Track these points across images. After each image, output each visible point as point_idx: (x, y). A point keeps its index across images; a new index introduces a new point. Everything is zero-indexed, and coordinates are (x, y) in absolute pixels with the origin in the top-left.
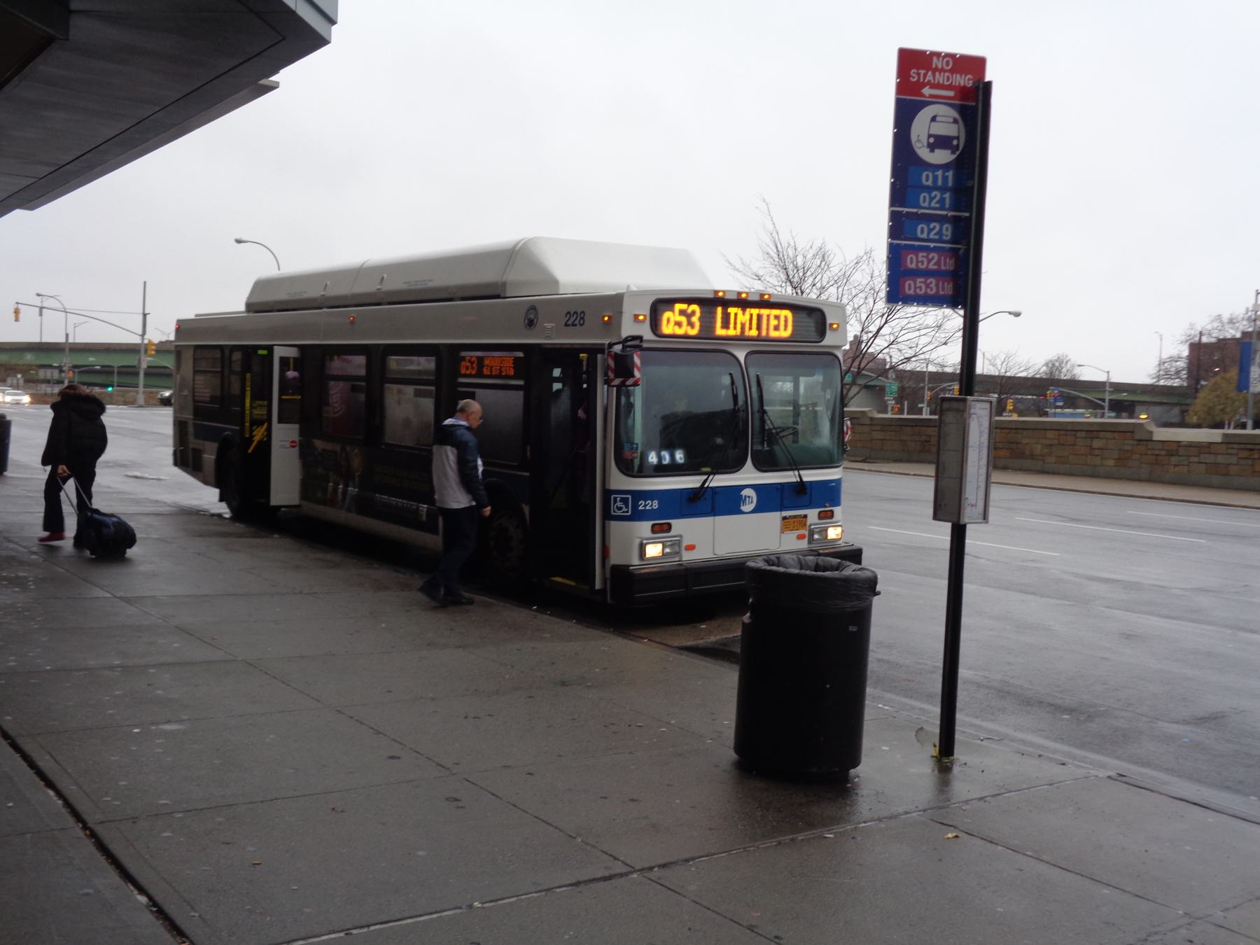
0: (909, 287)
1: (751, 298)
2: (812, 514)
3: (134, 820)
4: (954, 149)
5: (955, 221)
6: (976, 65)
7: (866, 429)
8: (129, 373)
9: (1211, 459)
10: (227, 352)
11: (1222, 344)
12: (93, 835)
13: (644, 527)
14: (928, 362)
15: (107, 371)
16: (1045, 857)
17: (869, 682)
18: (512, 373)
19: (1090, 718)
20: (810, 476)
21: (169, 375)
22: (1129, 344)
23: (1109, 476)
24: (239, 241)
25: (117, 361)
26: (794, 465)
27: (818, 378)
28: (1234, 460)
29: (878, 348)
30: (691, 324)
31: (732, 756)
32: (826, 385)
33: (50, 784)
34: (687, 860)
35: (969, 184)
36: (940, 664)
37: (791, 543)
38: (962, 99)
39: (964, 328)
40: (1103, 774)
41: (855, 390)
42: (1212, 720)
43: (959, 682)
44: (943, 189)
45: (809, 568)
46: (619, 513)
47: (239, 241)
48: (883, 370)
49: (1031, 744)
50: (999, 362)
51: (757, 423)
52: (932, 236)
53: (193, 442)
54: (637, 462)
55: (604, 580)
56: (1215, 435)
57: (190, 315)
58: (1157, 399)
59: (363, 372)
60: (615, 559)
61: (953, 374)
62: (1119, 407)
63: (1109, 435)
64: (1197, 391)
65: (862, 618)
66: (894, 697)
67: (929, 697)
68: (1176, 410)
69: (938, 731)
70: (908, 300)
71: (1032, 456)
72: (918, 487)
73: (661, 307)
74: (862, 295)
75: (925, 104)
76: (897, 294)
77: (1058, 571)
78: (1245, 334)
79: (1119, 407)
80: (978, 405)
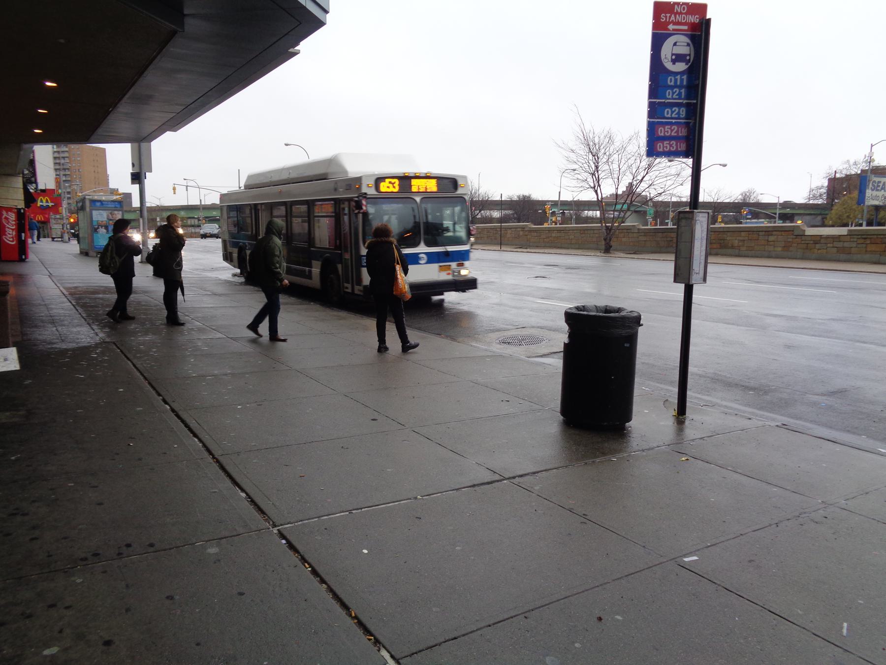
0: (660, 147)
3: (238, 453)
4: (687, 62)
5: (688, 106)
6: (703, 8)
7: (635, 235)
9: (840, 245)
11: (848, 178)
12: (218, 461)
14: (672, 195)
16: (739, 471)
19: (766, 393)
22: (792, 181)
24: (287, 145)
28: (854, 245)
29: (643, 189)
33: (195, 435)
34: (534, 473)
38: (692, 31)
40: (773, 424)
41: (628, 213)
42: (840, 393)
44: (680, 87)
47: (287, 145)
48: (646, 201)
49: (731, 408)
53: (230, 249)
56: (843, 231)
61: (686, 202)
62: (784, 217)
63: (779, 233)
64: (832, 205)
65: (632, 339)
66: (652, 383)
68: (819, 218)
70: (659, 155)
71: (733, 247)
72: (666, 266)
75: (671, 35)
76: (652, 152)
79: (784, 217)
80: (701, 215)
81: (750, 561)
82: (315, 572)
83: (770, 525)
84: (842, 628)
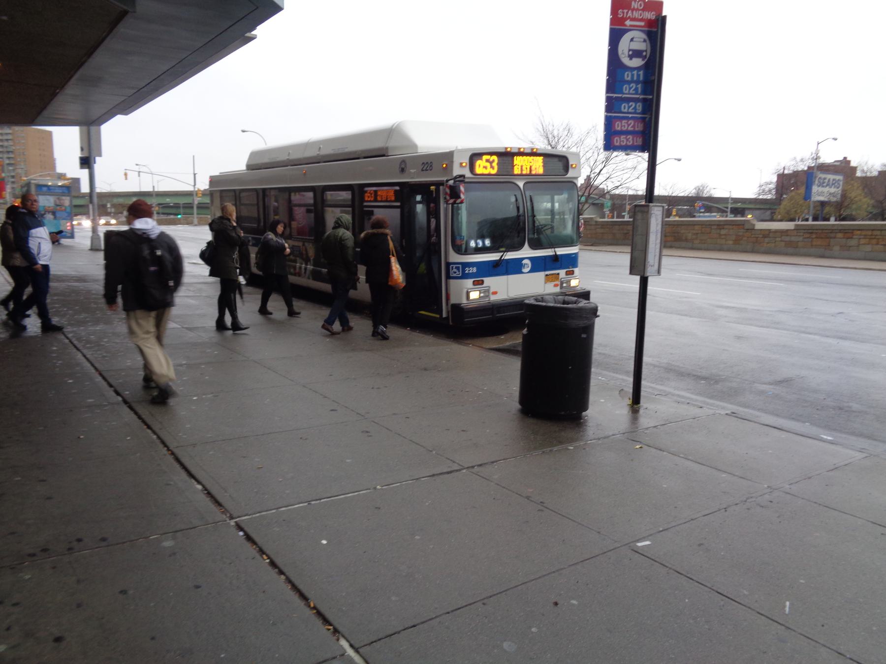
0: (617, 141)
1: (526, 151)
2: (562, 273)
3: (194, 445)
4: (644, 58)
5: (644, 101)
8: (189, 206)
9: (787, 239)
10: (237, 193)
11: (796, 174)
13: (469, 283)
14: (628, 188)
15: (177, 206)
17: (593, 366)
18: (393, 198)
19: (717, 382)
20: (561, 251)
21: (207, 208)
23: (729, 250)
24: (243, 131)
25: (182, 201)
26: (552, 246)
27: (565, 196)
28: (801, 239)
30: (492, 167)
31: (518, 406)
32: (569, 200)
33: (149, 427)
34: (493, 462)
35: (653, 78)
36: (633, 355)
37: (551, 289)
39: (648, 169)
40: (723, 412)
41: (586, 206)
42: (785, 382)
43: (644, 364)
44: (637, 82)
45: (559, 303)
46: (455, 275)
47: (243, 131)
48: (603, 194)
49: (683, 397)
50: (668, 188)
51: (531, 223)
52: (630, 110)
54: (464, 247)
55: (448, 312)
56: (790, 225)
57: (217, 173)
58: (758, 206)
59: (312, 202)
60: (453, 300)
61: (642, 195)
65: (589, 330)
67: (627, 373)
68: (768, 213)
69: (631, 391)
70: (616, 148)
71: (686, 240)
72: (622, 258)
73: (475, 158)
74: (591, 151)
76: (609, 146)
77: (699, 305)
78: (809, 168)
80: (656, 208)
81: (700, 545)
82: (273, 564)
83: (719, 510)
84: (785, 606)
